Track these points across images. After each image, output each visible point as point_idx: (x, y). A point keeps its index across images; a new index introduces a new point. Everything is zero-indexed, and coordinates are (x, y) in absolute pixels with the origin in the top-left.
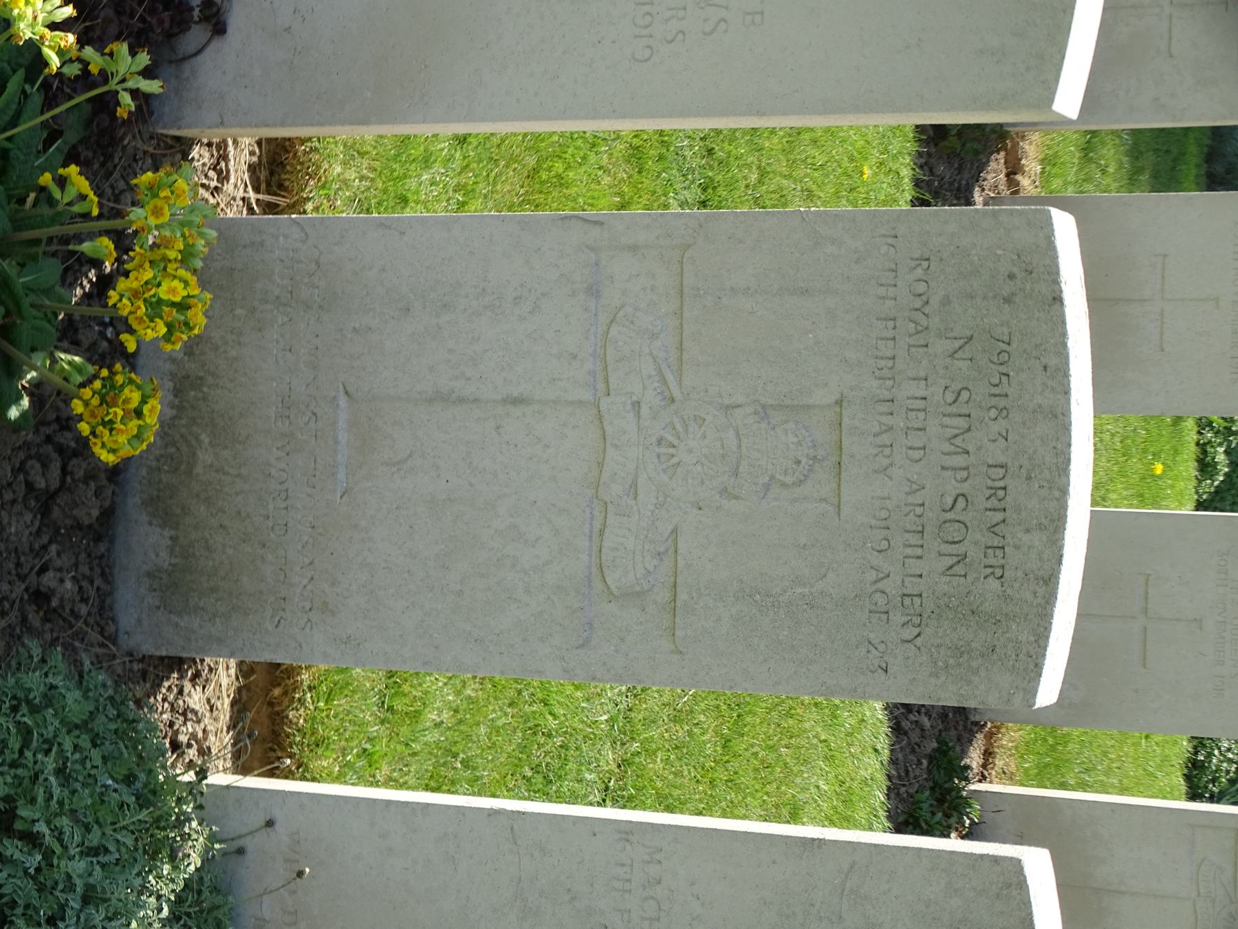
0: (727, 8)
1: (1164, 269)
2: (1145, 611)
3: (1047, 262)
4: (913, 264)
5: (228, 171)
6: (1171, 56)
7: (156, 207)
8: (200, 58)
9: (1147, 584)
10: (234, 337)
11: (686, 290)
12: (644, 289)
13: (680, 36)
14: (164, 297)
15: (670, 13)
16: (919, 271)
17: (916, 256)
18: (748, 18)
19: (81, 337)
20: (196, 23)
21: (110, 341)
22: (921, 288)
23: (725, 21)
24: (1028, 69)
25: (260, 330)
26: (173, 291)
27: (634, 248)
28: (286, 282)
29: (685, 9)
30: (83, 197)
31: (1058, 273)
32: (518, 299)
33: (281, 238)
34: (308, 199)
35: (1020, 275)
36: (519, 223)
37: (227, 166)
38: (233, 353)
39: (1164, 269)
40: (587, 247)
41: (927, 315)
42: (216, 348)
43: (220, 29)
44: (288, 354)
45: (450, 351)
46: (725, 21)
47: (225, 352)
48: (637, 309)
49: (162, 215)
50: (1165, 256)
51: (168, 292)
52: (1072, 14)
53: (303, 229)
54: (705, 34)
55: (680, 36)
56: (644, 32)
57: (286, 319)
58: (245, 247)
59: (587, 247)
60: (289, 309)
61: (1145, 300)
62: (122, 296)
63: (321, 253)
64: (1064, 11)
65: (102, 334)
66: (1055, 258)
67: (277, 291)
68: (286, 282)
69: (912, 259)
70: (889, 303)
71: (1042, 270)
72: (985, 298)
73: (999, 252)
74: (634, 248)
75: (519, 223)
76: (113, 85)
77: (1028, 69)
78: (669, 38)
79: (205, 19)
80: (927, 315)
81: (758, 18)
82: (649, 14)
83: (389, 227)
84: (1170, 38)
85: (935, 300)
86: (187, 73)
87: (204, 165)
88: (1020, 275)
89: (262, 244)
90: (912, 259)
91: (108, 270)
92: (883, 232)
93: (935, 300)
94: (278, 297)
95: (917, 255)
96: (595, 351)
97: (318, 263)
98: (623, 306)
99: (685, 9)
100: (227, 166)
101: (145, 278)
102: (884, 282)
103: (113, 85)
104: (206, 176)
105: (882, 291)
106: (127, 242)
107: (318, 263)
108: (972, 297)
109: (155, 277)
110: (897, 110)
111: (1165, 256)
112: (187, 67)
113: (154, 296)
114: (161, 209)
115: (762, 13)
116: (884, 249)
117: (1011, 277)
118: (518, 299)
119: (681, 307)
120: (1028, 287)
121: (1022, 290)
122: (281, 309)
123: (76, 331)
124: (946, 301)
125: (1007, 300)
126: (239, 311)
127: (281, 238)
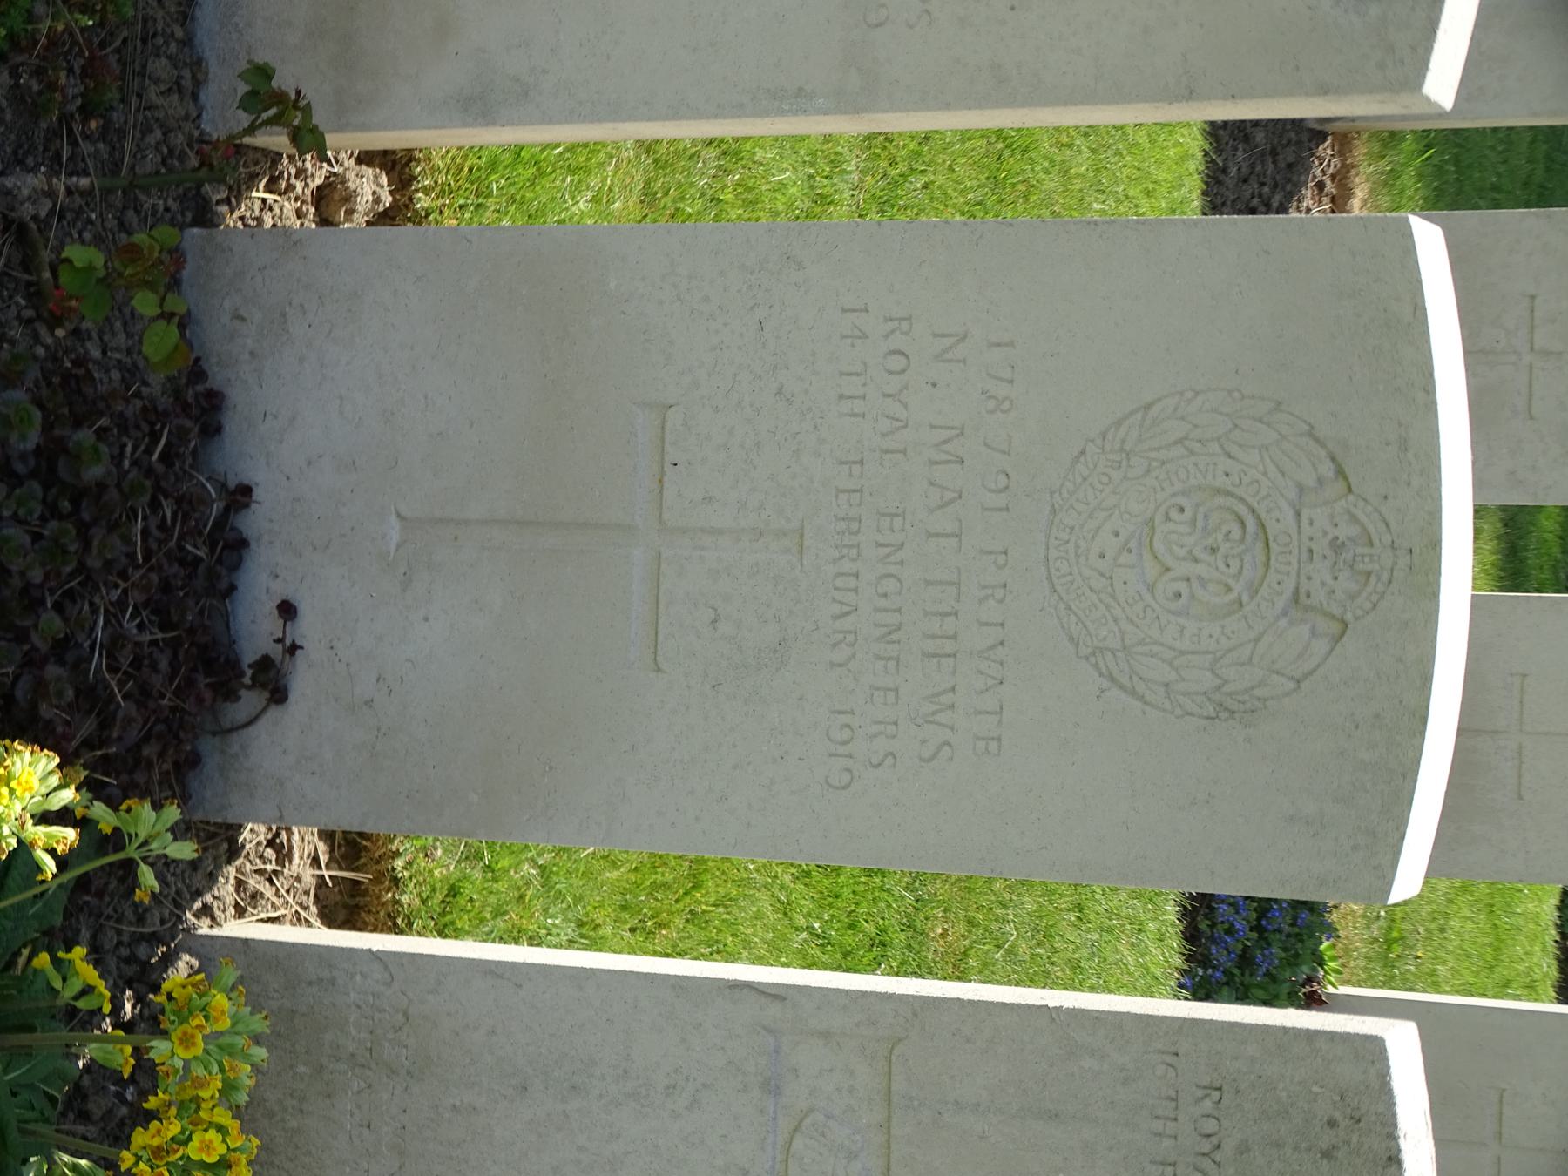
0: (952, 728)
1: (1522, 691)
2: (1499, 1135)
3: (1381, 1108)
4: (1200, 1093)
5: (291, 848)
6: (1531, 418)
7: (185, 1033)
8: (251, 728)
9: (1501, 1102)
10: (295, 1102)
11: (895, 1099)
12: (839, 1090)
13: (890, 760)
14: (195, 1157)
15: (876, 728)
16: (1208, 1104)
17: (1205, 1083)
18: (981, 744)
19: (91, 1106)
20: (249, 688)
21: (131, 1105)
22: (1210, 1126)
23: (949, 745)
24: (1355, 848)
25: (329, 1096)
26: (207, 1147)
27: (826, 1035)
28: (363, 1035)
29: (896, 724)
30: (88, 990)
31: (1394, 1124)
32: (670, 1089)
33: (358, 978)
34: (397, 854)
35: (1344, 1123)
36: (673, 987)
37: (289, 840)
38: (294, 1124)
39: (1522, 691)
40: (764, 1028)
41: (1218, 1164)
42: (271, 1115)
43: (279, 695)
44: (366, 1131)
45: (580, 1149)
46: (949, 745)
47: (283, 1120)
48: (829, 1116)
49: (194, 1044)
50: (1525, 676)
51: (201, 1150)
52: (1415, 781)
53: (386, 968)
54: (922, 760)
55: (890, 760)
56: (842, 750)
57: (363, 1085)
58: (310, 983)
59: (764, 1028)
60: (368, 1073)
61: (1495, 732)
62: (139, 1159)
63: (410, 1001)
64: (1404, 776)
65: (120, 1097)
66: (1390, 1103)
67: (351, 1047)
68: (363, 1035)
69: (1198, 1086)
70: (1167, 1143)
71: (1373, 1118)
72: (1296, 1148)
73: (1315, 1089)
74: (826, 1035)
75: (673, 987)
76: (131, 852)
77: (1355, 848)
78: (875, 761)
79: (256, 684)
80: (1218, 1164)
81: (993, 745)
82: (848, 726)
83: (500, 977)
84: (1530, 395)
85: (1229, 1145)
86: (236, 748)
87: (259, 844)
88: (1344, 1123)
89: (332, 981)
90: (1198, 1086)
91: (128, 1016)
92: (1160, 1046)
93: (1229, 1145)
94: (353, 1055)
95: (1206, 1081)
96: (773, 1167)
97: (406, 1015)
98: (811, 1110)
99: (896, 724)
100: (289, 840)
101: (170, 1135)
102: (1160, 1112)
103: (131, 852)
104: (261, 857)
105: (1158, 1126)
106: (154, 977)
107: (406, 1015)
108: (1278, 1145)
109: (183, 1132)
110: (1172, 97)
111: (1525, 676)
112: (235, 737)
113: (181, 1158)
114: (193, 1036)
115: (999, 739)
116: (1160, 1070)
117: (1332, 1123)
118: (670, 1089)
119: (889, 1118)
120: (1355, 1139)
121: (1347, 1142)
122: (357, 1070)
123: (85, 1097)
124: (1243, 1148)
125: (1327, 1155)
126: (302, 1069)
127: (358, 978)
